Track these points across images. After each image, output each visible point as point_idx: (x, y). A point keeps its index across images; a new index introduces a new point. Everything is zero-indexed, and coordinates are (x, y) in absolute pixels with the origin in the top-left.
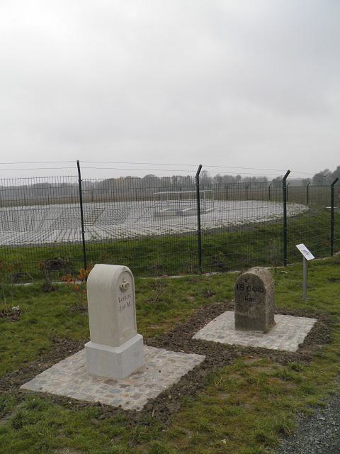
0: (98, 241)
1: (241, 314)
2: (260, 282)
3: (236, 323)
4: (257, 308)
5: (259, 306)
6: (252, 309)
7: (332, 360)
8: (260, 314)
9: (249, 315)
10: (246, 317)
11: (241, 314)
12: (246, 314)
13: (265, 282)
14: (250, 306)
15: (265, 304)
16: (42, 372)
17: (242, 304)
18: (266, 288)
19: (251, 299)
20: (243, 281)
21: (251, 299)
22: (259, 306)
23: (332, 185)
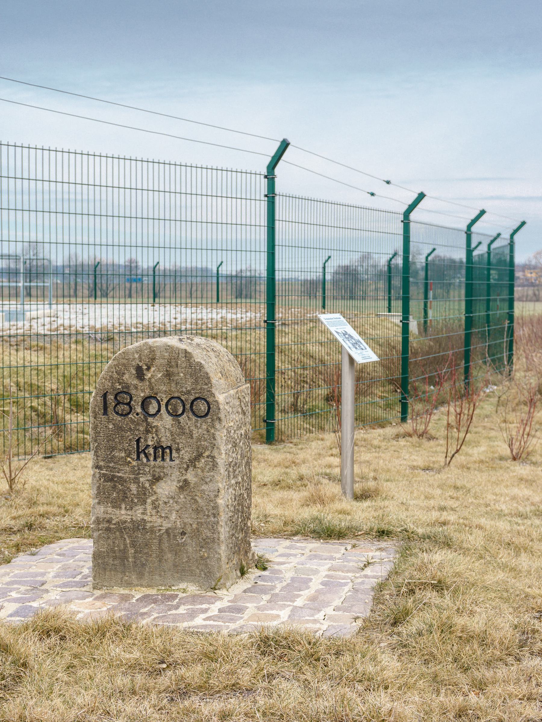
0: (446, 263)
1: (123, 514)
2: (198, 373)
3: (97, 556)
4: (185, 486)
5: (190, 476)
6: (166, 489)
7: (432, 469)
8: (198, 511)
9: (153, 519)
10: (139, 526)
11: (123, 514)
12: (138, 513)
13: (216, 379)
14: (156, 479)
15: (215, 465)
16: (219, 409)
17: (124, 473)
18: (221, 398)
19: (161, 451)
20: (129, 378)
21: (161, 451)
22: (190, 476)
23: (469, 226)
